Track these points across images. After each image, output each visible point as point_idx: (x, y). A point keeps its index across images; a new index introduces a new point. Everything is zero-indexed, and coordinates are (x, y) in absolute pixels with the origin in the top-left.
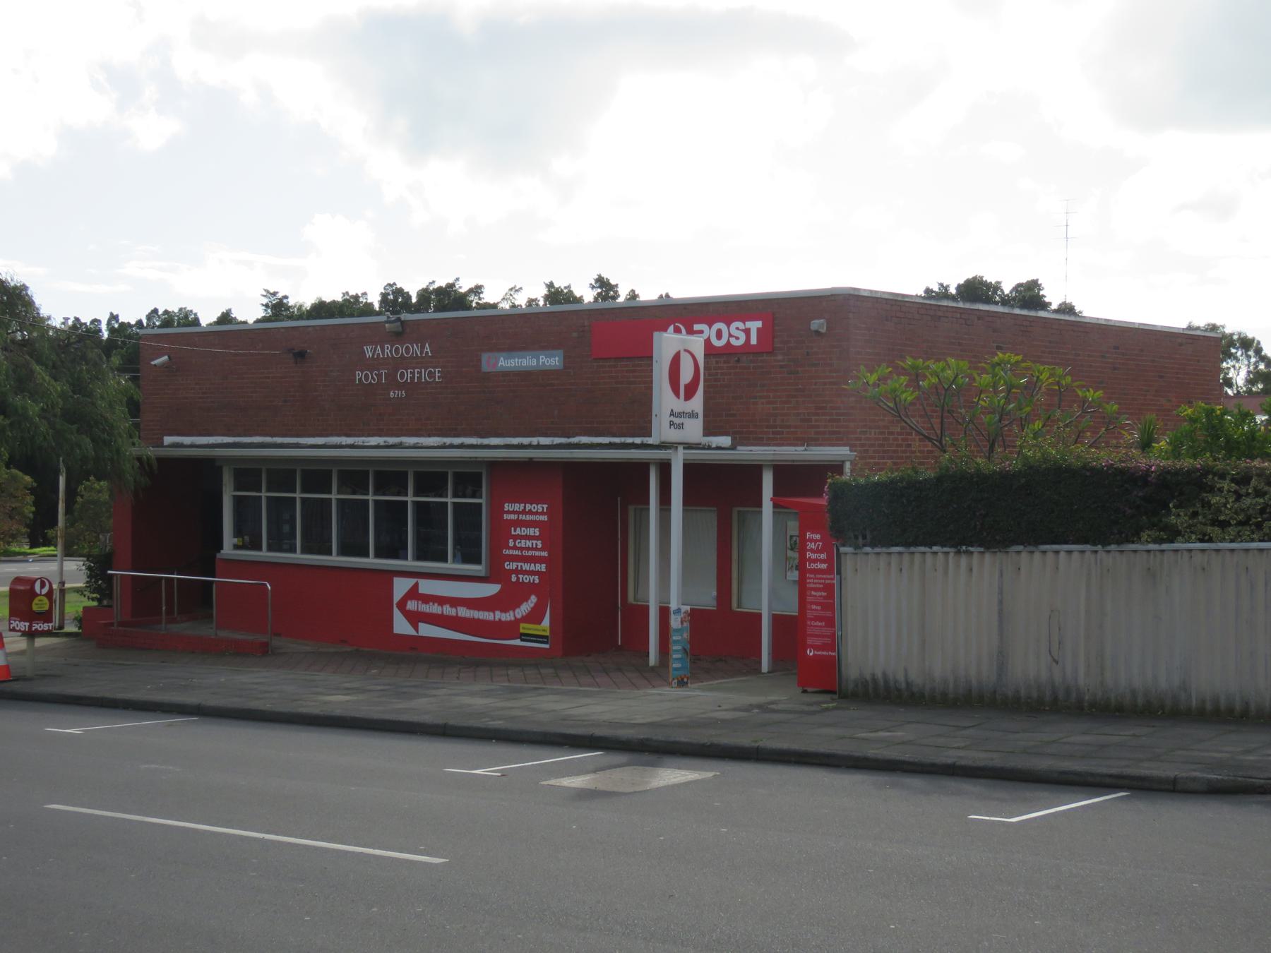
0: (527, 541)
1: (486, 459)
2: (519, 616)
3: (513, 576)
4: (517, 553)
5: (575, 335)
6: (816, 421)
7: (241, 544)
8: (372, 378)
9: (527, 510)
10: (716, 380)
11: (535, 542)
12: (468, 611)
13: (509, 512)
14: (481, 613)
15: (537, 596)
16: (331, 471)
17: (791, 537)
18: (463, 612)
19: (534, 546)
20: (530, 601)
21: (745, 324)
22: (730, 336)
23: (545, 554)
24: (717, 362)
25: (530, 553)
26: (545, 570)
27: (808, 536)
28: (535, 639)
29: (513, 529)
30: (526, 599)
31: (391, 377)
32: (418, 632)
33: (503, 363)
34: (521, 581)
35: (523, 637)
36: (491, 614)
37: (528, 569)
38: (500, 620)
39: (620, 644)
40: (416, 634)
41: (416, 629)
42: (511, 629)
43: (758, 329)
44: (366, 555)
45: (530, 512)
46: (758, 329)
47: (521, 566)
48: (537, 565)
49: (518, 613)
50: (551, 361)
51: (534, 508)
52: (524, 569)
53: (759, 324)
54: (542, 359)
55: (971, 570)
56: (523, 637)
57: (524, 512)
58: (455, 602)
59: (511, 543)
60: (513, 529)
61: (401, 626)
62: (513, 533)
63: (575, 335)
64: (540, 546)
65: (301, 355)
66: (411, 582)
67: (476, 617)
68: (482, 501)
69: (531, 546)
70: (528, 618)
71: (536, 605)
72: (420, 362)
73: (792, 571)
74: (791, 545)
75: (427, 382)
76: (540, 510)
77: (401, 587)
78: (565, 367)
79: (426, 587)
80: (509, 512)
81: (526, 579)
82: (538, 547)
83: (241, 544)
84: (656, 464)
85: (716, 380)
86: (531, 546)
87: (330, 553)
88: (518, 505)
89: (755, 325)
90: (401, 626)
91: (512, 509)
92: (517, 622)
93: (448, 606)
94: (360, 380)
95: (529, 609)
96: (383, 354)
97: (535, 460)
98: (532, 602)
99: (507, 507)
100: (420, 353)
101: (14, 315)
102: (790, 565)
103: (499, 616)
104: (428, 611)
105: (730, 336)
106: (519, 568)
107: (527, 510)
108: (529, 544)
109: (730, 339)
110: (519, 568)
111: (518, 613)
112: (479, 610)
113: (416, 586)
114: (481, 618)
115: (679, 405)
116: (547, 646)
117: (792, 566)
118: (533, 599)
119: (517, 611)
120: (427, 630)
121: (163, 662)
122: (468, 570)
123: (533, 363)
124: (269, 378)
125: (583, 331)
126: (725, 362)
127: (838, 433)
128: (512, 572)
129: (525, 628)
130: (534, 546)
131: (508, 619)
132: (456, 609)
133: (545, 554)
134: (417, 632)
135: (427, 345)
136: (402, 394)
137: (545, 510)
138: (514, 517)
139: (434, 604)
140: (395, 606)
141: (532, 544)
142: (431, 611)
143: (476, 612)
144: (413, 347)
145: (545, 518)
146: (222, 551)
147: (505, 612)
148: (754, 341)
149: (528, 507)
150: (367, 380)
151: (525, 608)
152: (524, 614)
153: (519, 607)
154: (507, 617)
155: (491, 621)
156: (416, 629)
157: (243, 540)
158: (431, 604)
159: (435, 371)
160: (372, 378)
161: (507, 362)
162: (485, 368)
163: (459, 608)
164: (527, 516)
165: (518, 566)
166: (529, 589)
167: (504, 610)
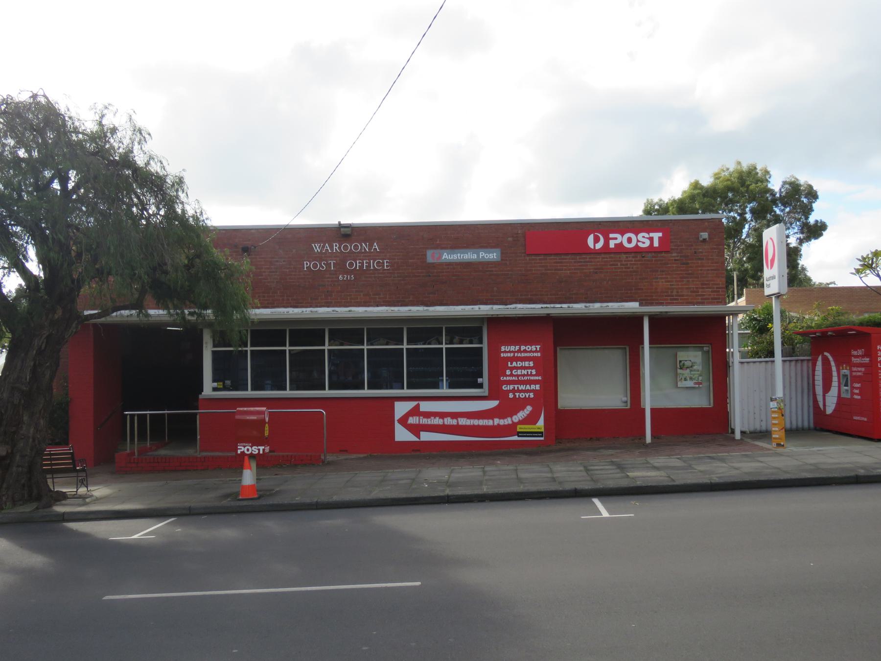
0: (523, 370)
1: (506, 316)
5: (510, 239)
9: (522, 350)
11: (529, 371)
13: (505, 352)
16: (403, 328)
17: (680, 361)
18: (463, 421)
19: (529, 373)
22: (638, 241)
24: (627, 258)
25: (526, 378)
28: (525, 435)
29: (509, 363)
30: (523, 408)
33: (447, 257)
34: (517, 397)
37: (524, 389)
42: (511, 429)
43: (659, 238)
45: (525, 351)
47: (518, 387)
48: (532, 386)
50: (492, 256)
53: (660, 234)
54: (445, 256)
55: (771, 375)
56: (519, 434)
58: (455, 415)
59: (508, 372)
60: (509, 363)
61: (402, 434)
62: (509, 365)
63: (510, 239)
66: (410, 405)
69: (526, 373)
71: (531, 412)
74: (680, 366)
76: (534, 349)
77: (401, 409)
78: (502, 260)
79: (425, 406)
80: (505, 352)
81: (522, 395)
86: (526, 373)
87: (285, 389)
89: (656, 236)
90: (402, 434)
91: (507, 350)
92: (515, 425)
94: (374, 266)
97: (551, 315)
99: (503, 349)
101: (178, 198)
102: (680, 378)
104: (429, 423)
105: (638, 241)
106: (516, 389)
108: (524, 372)
110: (516, 389)
112: (479, 419)
113: (418, 406)
116: (542, 439)
117: (682, 379)
118: (529, 409)
119: (514, 417)
120: (426, 436)
121: (276, 475)
122: (419, 393)
123: (475, 256)
125: (517, 237)
126: (633, 257)
127: (719, 299)
128: (510, 391)
129: (520, 428)
130: (529, 373)
131: (506, 423)
132: (493, 420)
134: (420, 439)
135: (375, 244)
136: (351, 278)
137: (538, 349)
141: (528, 372)
144: (361, 246)
145: (539, 355)
146: (203, 393)
148: (656, 244)
149: (523, 348)
154: (508, 421)
155: (491, 426)
156: (419, 437)
161: (447, 256)
162: (430, 259)
165: (514, 387)
166: (526, 402)
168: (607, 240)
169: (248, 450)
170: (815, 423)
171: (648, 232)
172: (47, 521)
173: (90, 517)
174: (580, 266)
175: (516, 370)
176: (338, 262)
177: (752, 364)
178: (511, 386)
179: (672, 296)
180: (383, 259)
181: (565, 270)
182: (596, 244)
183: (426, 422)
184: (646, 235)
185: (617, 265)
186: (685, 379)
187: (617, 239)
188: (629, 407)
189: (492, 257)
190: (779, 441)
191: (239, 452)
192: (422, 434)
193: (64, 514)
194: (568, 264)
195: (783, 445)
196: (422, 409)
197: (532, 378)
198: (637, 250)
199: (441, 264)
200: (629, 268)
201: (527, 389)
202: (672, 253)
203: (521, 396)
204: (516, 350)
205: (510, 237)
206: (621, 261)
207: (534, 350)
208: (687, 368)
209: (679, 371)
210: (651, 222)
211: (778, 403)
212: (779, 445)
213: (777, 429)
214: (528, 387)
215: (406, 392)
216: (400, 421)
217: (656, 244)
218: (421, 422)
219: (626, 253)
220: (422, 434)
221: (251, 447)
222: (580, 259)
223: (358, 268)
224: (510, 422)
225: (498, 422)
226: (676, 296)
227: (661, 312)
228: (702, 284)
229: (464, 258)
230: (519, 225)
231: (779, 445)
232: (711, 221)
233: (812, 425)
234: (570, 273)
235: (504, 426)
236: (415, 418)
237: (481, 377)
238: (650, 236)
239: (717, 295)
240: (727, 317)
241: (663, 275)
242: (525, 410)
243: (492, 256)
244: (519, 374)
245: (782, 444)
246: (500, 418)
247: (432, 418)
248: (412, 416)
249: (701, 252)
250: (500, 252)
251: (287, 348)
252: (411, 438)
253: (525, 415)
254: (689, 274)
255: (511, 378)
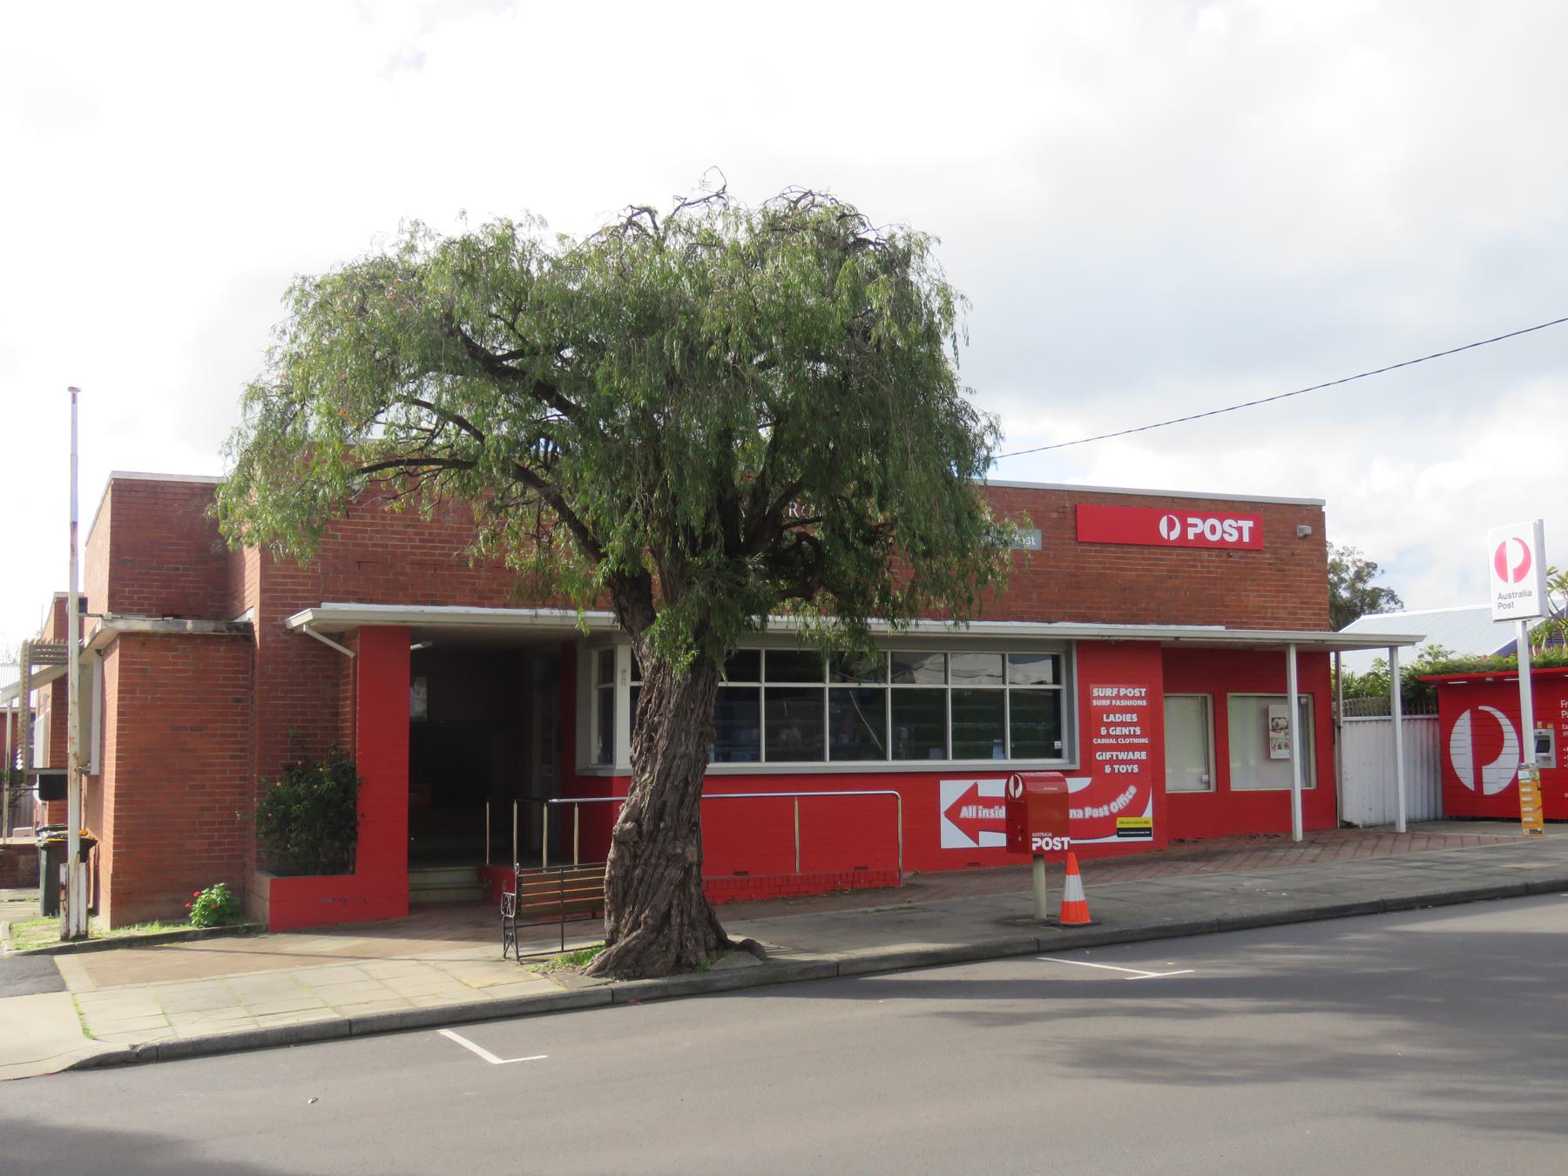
0: (1124, 728)
2: (1115, 810)
5: (1054, 515)
6: (1301, 614)
10: (1209, 572)
11: (1132, 729)
13: (1099, 698)
19: (1132, 733)
23: (1145, 741)
24: (1209, 556)
25: (1128, 741)
27: (1562, 704)
29: (1105, 716)
30: (1124, 790)
34: (1116, 771)
35: (1121, 832)
36: (1080, 811)
37: (1125, 758)
38: (1091, 817)
40: (975, 845)
41: (976, 840)
43: (1250, 528)
44: (821, 758)
45: (1126, 697)
46: (1250, 528)
47: (1117, 756)
48: (1136, 753)
49: (1114, 807)
51: (1130, 692)
52: (1120, 758)
53: (1251, 524)
56: (1121, 832)
57: (1118, 697)
59: (1103, 731)
60: (1105, 716)
61: (952, 837)
62: (1105, 720)
63: (1054, 515)
66: (963, 786)
69: (1127, 733)
70: (1125, 812)
71: (1135, 796)
73: (1275, 750)
76: (1138, 695)
77: (950, 792)
80: (1099, 698)
81: (1123, 769)
84: (1297, 644)
85: (1209, 572)
86: (1127, 733)
89: (1247, 525)
91: (1103, 694)
92: (1113, 817)
97: (1181, 639)
98: (1130, 794)
104: (992, 816)
106: (1114, 758)
108: (1125, 731)
110: (1114, 758)
113: (975, 788)
115: (1511, 586)
118: (1132, 790)
119: (1113, 804)
122: (977, 765)
125: (1063, 512)
128: (1105, 762)
129: (1122, 823)
130: (1132, 733)
131: (1102, 815)
133: (1145, 741)
134: (978, 844)
137: (1143, 695)
138: (1106, 703)
139: (1000, 808)
141: (1130, 731)
142: (997, 817)
145: (1144, 703)
147: (1097, 807)
148: (1246, 538)
149: (1123, 692)
151: (1122, 801)
154: (1102, 812)
156: (976, 840)
165: (1112, 756)
166: (1129, 779)
168: (1185, 526)
169: (1047, 844)
170: (1446, 809)
171: (1236, 520)
172: (811, 980)
173: (884, 966)
174: (1149, 565)
175: (1114, 728)
178: (1108, 753)
179: (1265, 618)
181: (1130, 570)
183: (987, 815)
185: (1196, 566)
186: (1280, 748)
187: (1199, 527)
188: (1212, 790)
190: (1534, 826)
191: (1034, 847)
192: (983, 835)
193: (838, 964)
194: (1133, 562)
195: (1541, 832)
196: (981, 794)
197: (1136, 741)
198: (1222, 546)
201: (1129, 758)
203: (1121, 770)
204: (1114, 695)
205: (1054, 512)
207: (1135, 695)
208: (1281, 729)
209: (1272, 734)
210: (1237, 504)
211: (1531, 771)
212: (1534, 831)
213: (1530, 809)
214: (1131, 756)
215: (951, 764)
216: (949, 814)
218: (980, 816)
220: (983, 835)
221: (1052, 838)
224: (1107, 813)
225: (1090, 813)
226: (1272, 618)
227: (1316, 640)
228: (1302, 603)
230: (1066, 493)
231: (1534, 831)
232: (1309, 508)
233: (1440, 815)
235: (1100, 819)
236: (970, 808)
237: (1059, 738)
239: (1320, 620)
240: (1332, 655)
242: (1127, 793)
244: (1118, 734)
245: (1539, 829)
246: (1093, 807)
248: (967, 804)
249: (1299, 554)
250: (1040, 536)
251: (763, 685)
252: (967, 843)
253: (1128, 802)
254: (1286, 586)
255: (1106, 741)
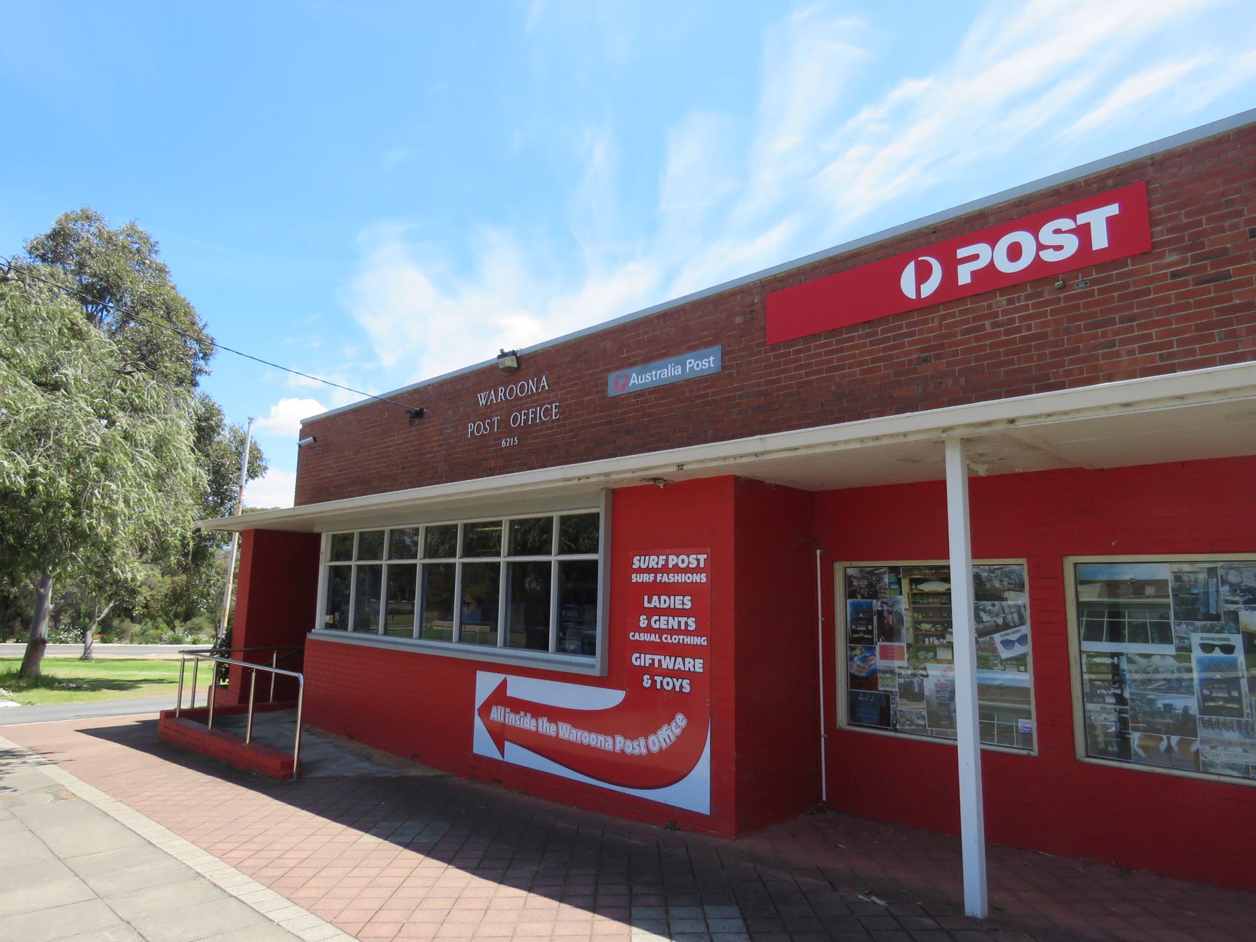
3: (646, 677)
4: (654, 638)
5: (739, 320)
7: (331, 622)
8: (485, 429)
9: (670, 566)
11: (683, 620)
12: (573, 731)
13: (640, 571)
14: (593, 736)
15: (687, 716)
18: (567, 732)
19: (683, 627)
20: (673, 724)
21: (1075, 220)
22: (1041, 247)
23: (701, 641)
24: (1010, 301)
25: (675, 639)
26: (701, 670)
29: (646, 597)
31: (504, 422)
32: (503, 755)
33: (636, 381)
36: (609, 739)
37: (671, 667)
38: (623, 751)
39: (824, 798)
41: (501, 749)
43: (1110, 220)
45: (677, 570)
46: (1110, 220)
47: (660, 661)
48: (687, 660)
50: (704, 363)
58: (555, 714)
59: (643, 622)
60: (646, 597)
61: (483, 745)
62: (646, 605)
64: (692, 627)
65: (419, 414)
66: (498, 677)
67: (586, 742)
68: (598, 556)
69: (676, 627)
72: (535, 400)
75: (543, 423)
76: (694, 565)
77: (486, 684)
79: (520, 688)
80: (640, 571)
81: (668, 684)
82: (689, 628)
83: (331, 622)
86: (676, 627)
88: (655, 558)
89: (1098, 219)
90: (483, 745)
93: (545, 719)
95: (673, 738)
96: (497, 399)
99: (637, 562)
100: (536, 390)
103: (620, 744)
105: (1041, 247)
107: (670, 566)
108: (673, 623)
109: (1040, 253)
110: (656, 665)
111: (654, 743)
113: (503, 686)
114: (593, 744)
118: (681, 720)
119: (652, 738)
120: (516, 755)
123: (678, 371)
124: (390, 446)
128: (643, 670)
130: (683, 627)
131: (637, 752)
133: (701, 641)
137: (702, 565)
138: (648, 578)
140: (476, 712)
141: (679, 623)
143: (586, 734)
145: (702, 578)
149: (673, 560)
150: (478, 431)
152: (664, 745)
153: (655, 732)
157: (334, 617)
158: (522, 714)
159: (552, 408)
160: (485, 429)
161: (640, 379)
162: (612, 392)
163: (560, 724)
164: (671, 575)
165: (653, 660)
166: (676, 702)
167: (631, 735)
174: (885, 349)
175: (657, 618)
176: (503, 417)
177: (1051, 250)
180: (551, 404)
182: (922, 286)
184: (1066, 224)
185: (983, 327)
189: (707, 364)
196: (510, 692)
197: (688, 640)
199: (628, 397)
200: (1018, 330)
202: (1161, 255)
206: (996, 314)
214: (679, 664)
217: (1100, 240)
219: (1004, 290)
222: (884, 332)
223: (522, 425)
229: (662, 377)
234: (862, 372)
238: (1079, 223)
241: (1130, 329)
243: (704, 363)
247: (522, 714)
